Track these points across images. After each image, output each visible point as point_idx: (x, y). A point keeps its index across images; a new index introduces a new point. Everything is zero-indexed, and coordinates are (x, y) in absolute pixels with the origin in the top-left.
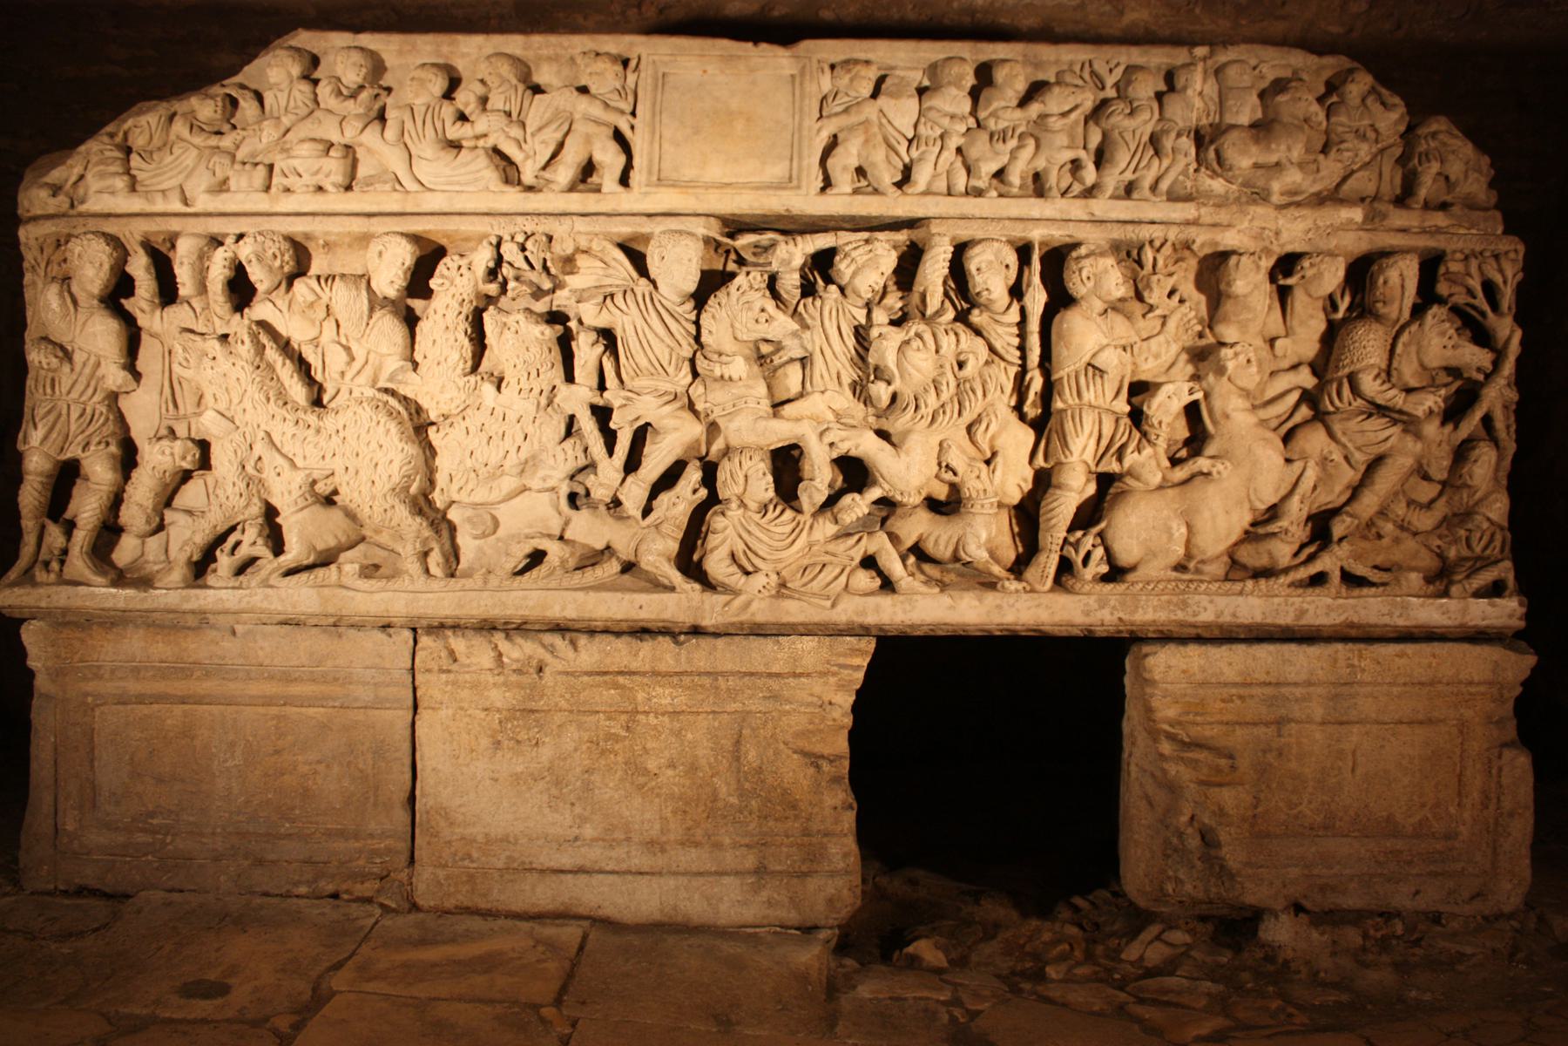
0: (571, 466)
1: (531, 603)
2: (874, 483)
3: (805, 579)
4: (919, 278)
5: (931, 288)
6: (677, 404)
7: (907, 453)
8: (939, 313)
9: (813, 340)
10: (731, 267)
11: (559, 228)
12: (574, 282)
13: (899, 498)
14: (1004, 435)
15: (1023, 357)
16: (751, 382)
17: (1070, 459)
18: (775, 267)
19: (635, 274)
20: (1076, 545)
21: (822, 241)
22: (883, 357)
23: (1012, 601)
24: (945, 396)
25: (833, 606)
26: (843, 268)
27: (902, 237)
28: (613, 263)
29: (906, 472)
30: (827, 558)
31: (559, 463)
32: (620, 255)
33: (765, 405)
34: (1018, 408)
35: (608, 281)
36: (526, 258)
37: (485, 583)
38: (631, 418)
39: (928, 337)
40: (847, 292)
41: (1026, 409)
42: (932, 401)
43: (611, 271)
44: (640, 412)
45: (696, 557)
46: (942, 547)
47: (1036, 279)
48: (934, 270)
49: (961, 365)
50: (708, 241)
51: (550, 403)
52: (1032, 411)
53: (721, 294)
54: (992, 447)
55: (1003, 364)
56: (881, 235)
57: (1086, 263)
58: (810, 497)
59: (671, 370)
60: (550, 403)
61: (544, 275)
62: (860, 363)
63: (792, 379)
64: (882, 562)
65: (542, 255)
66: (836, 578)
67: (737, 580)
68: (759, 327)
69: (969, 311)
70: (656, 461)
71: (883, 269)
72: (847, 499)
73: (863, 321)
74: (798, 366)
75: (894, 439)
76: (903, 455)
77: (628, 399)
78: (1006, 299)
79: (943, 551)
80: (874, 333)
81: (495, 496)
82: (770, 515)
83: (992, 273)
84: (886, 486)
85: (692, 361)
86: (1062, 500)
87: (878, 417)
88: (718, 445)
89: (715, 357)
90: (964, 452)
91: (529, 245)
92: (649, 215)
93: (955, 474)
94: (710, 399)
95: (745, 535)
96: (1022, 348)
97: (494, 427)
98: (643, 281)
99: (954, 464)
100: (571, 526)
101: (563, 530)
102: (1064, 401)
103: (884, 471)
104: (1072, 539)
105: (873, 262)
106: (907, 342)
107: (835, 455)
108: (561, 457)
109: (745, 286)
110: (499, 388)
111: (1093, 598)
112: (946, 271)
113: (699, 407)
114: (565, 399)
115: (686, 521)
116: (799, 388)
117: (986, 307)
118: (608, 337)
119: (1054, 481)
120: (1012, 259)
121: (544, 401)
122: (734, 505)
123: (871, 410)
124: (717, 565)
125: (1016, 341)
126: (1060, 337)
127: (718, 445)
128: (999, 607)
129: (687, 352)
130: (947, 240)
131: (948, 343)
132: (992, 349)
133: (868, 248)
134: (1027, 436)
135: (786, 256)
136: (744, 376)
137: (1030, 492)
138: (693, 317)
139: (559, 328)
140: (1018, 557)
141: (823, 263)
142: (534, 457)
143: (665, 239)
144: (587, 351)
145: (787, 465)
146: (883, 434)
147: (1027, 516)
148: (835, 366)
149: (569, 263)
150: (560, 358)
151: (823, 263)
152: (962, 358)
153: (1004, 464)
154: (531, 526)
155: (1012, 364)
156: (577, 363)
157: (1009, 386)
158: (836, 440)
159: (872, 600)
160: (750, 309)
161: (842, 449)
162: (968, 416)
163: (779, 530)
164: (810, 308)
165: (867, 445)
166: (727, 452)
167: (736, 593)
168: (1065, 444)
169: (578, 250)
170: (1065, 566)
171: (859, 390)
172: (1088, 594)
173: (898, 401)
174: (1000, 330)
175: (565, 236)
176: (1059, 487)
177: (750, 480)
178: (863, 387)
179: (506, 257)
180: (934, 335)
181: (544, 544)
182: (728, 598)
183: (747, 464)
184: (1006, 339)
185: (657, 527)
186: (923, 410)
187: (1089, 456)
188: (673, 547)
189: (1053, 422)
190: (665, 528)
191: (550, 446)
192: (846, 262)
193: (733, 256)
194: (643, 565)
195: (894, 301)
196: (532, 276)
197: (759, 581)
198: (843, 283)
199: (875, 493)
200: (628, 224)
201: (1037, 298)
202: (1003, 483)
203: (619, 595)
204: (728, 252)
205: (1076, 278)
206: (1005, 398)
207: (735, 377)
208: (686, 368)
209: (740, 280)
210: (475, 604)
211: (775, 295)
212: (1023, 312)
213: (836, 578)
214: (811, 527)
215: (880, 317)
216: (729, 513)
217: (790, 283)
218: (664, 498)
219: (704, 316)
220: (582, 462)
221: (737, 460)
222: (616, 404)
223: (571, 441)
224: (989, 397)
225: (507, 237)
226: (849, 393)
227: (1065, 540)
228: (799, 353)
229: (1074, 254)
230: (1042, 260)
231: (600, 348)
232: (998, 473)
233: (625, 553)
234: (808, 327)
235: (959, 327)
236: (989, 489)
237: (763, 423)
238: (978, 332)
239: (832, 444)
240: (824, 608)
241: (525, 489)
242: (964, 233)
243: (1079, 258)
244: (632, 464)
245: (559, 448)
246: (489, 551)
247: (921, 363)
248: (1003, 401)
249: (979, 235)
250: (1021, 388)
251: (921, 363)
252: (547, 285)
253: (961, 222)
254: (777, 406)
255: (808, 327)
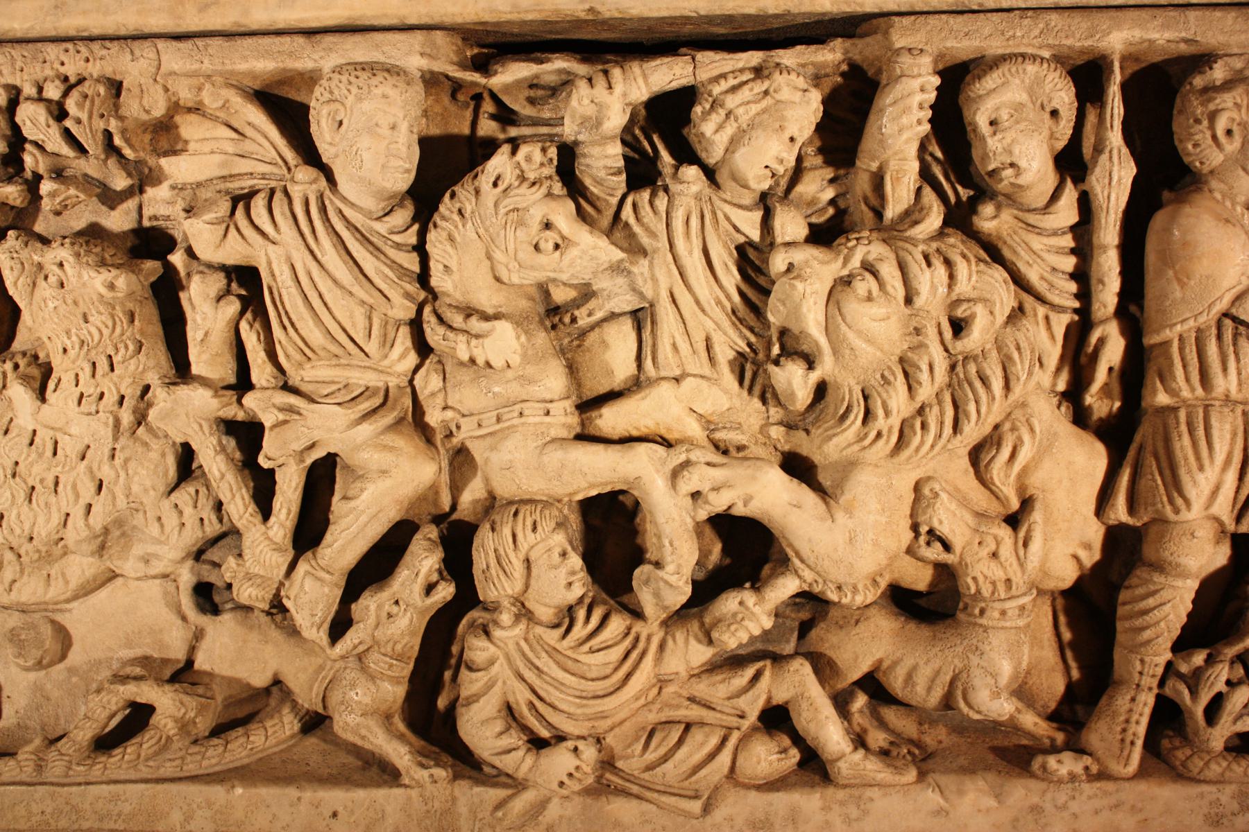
0: (192, 536)
1: (127, 808)
2: (783, 563)
3: (651, 756)
4: (869, 143)
5: (893, 165)
6: (388, 418)
7: (849, 511)
8: (912, 215)
9: (655, 277)
10: (488, 127)
11: (133, 67)
12: (178, 169)
13: (833, 596)
14: (1047, 464)
15: (1085, 295)
16: (530, 370)
17: (1185, 515)
18: (569, 130)
19: (290, 155)
20: (1194, 681)
21: (666, 74)
22: (796, 311)
23: (1062, 798)
24: (925, 392)
25: (707, 809)
26: (711, 131)
27: (831, 55)
28: (249, 131)
29: (848, 543)
30: (694, 713)
31: (167, 535)
32: (256, 116)
33: (564, 418)
34: (1073, 397)
35: (244, 166)
36: (68, 136)
37: (39, 768)
38: (298, 446)
39: (889, 270)
40: (722, 177)
41: (1089, 400)
42: (899, 402)
43: (248, 146)
44: (316, 435)
45: (442, 703)
46: (920, 689)
47: (1115, 137)
48: (901, 127)
49: (958, 327)
50: (431, 81)
51: (141, 419)
52: (1099, 403)
53: (464, 191)
54: (1021, 489)
55: (1041, 310)
56: (788, 57)
57: (1226, 100)
58: (657, 595)
59: (372, 347)
60: (141, 419)
61: (112, 162)
62: (751, 319)
63: (617, 354)
64: (803, 720)
65: (101, 125)
66: (712, 756)
67: (520, 761)
68: (542, 259)
69: (971, 207)
70: (353, 528)
71: (792, 130)
72: (729, 603)
73: (755, 235)
74: (627, 326)
75: (825, 479)
76: (840, 516)
77: (291, 409)
78: (1050, 179)
79: (926, 693)
80: (778, 262)
81: (56, 591)
82: (579, 631)
83: (1020, 128)
84: (808, 575)
85: (416, 326)
86: (1165, 595)
87: (790, 426)
88: (472, 494)
89: (457, 320)
90: (964, 502)
91: (71, 105)
92: (310, 33)
93: (947, 547)
94: (453, 402)
95: (530, 675)
96: (1082, 277)
97: (37, 470)
98: (305, 173)
99: (944, 530)
100: (205, 645)
101: (192, 650)
102: (1168, 390)
103: (805, 551)
104: (1184, 668)
105: (773, 116)
106: (846, 282)
107: (703, 515)
108: (171, 520)
109: (510, 177)
110: (41, 395)
111: (1229, 789)
112: (926, 128)
113: (434, 417)
114: (166, 416)
115: (417, 642)
116: (631, 369)
117: (1011, 199)
118: (246, 282)
119: (1148, 551)
120: (1064, 96)
121: (127, 417)
122: (506, 618)
123: (775, 413)
124: (480, 728)
125: (1069, 263)
126: (1167, 259)
127: (472, 494)
128: (1036, 810)
129: (404, 310)
130: (926, 62)
131: (930, 282)
132: (1019, 281)
133: (760, 87)
134: (1088, 460)
135: (590, 110)
136: (515, 360)
137: (1097, 566)
138: (411, 238)
139: (152, 267)
140: (1070, 687)
141: (669, 117)
142: (119, 523)
143: (339, 84)
144: (208, 314)
145: (610, 534)
146: (798, 467)
147: (1092, 611)
148: (700, 325)
149: (164, 134)
150: (158, 329)
151: (669, 117)
152: (960, 312)
153: (1047, 521)
154: (129, 644)
155: (1060, 309)
156: (194, 335)
157: (1054, 353)
158: (705, 487)
159: (781, 800)
160: (521, 223)
161: (718, 503)
162: (973, 432)
163: (600, 658)
164: (646, 214)
165: (769, 495)
166: (491, 504)
167: (516, 784)
168: (1174, 484)
169: (175, 108)
170: (1167, 716)
171: (751, 371)
172: (1219, 781)
173: (830, 397)
174: (1037, 243)
175: (146, 81)
176: (1159, 567)
177: (537, 565)
178: (758, 365)
179: (28, 132)
180: (902, 267)
181: (148, 693)
182: (501, 793)
183: (527, 539)
184: (1047, 260)
185: (360, 658)
186: (880, 422)
187: (1224, 508)
188: (394, 692)
189: (1144, 432)
190: (376, 661)
191: (149, 500)
192: (716, 119)
193: (488, 107)
194: (338, 727)
195: (818, 187)
196: (90, 167)
197: (560, 761)
198: (711, 161)
199: (785, 588)
200: (267, 54)
201: (1115, 177)
202: (1045, 559)
203: (292, 792)
204: (478, 98)
205: (1202, 134)
206: (1044, 378)
207: (498, 363)
208: (404, 339)
209: (499, 163)
210: (21, 811)
211: (574, 187)
212: (1085, 204)
213: (712, 756)
214: (662, 646)
215: (790, 225)
216: (497, 633)
217: (604, 162)
218: (369, 605)
219: (432, 236)
220: (213, 528)
221: (507, 531)
222: (268, 420)
223: (189, 489)
224: (1017, 391)
225: (28, 90)
226: (730, 380)
227: (1169, 665)
228: (626, 302)
229: (1198, 81)
230: (1127, 88)
231: (232, 307)
232: (1036, 546)
233: (309, 699)
234: (644, 253)
235: (955, 243)
236: (1018, 579)
237: (555, 456)
238: (993, 252)
239: (696, 495)
240: (688, 815)
241: (113, 576)
242: (963, 41)
243: (1210, 90)
244: (309, 532)
245: (166, 504)
246: (55, 694)
247: (876, 325)
248: (1041, 381)
249: (996, 47)
250: (1078, 354)
251: (876, 325)
252: (120, 182)
253: (957, 22)
254: (589, 405)
255: (644, 253)
